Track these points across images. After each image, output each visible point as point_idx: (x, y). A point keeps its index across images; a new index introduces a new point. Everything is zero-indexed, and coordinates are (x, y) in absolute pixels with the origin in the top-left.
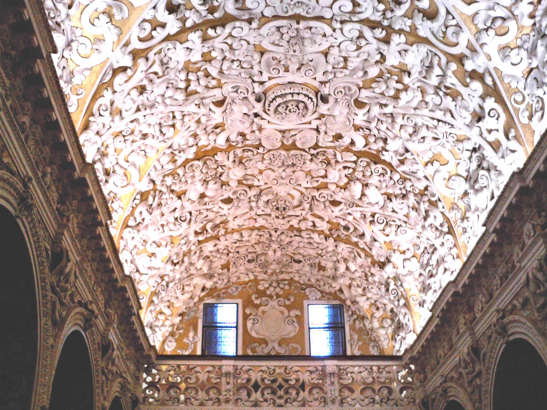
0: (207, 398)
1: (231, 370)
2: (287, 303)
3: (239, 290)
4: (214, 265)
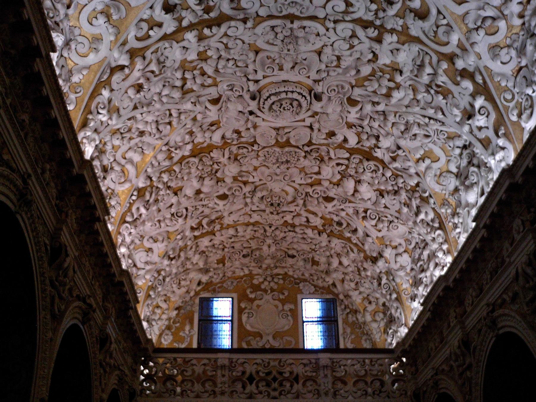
0: (203, 391)
1: (226, 362)
2: (281, 297)
3: (235, 284)
4: (210, 260)
